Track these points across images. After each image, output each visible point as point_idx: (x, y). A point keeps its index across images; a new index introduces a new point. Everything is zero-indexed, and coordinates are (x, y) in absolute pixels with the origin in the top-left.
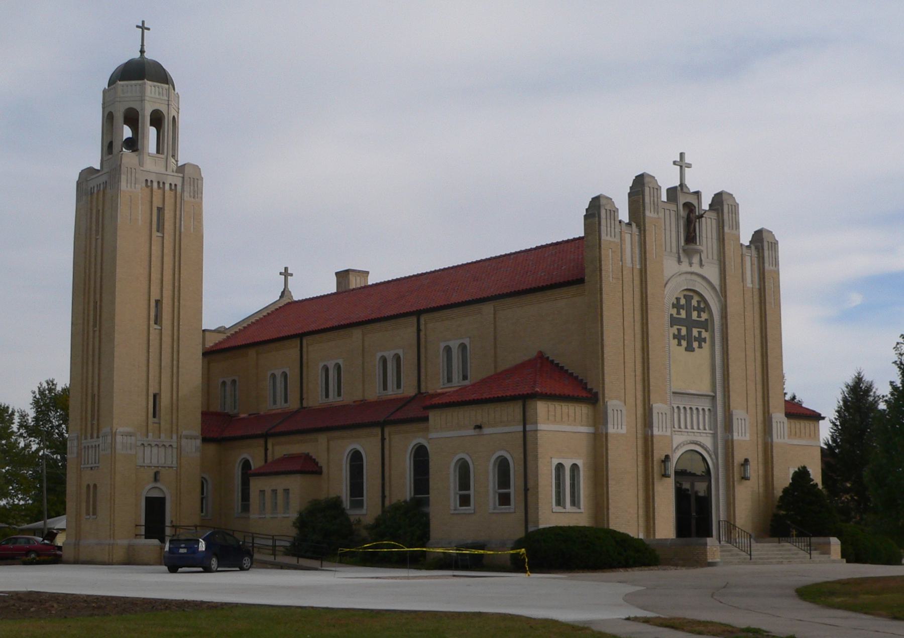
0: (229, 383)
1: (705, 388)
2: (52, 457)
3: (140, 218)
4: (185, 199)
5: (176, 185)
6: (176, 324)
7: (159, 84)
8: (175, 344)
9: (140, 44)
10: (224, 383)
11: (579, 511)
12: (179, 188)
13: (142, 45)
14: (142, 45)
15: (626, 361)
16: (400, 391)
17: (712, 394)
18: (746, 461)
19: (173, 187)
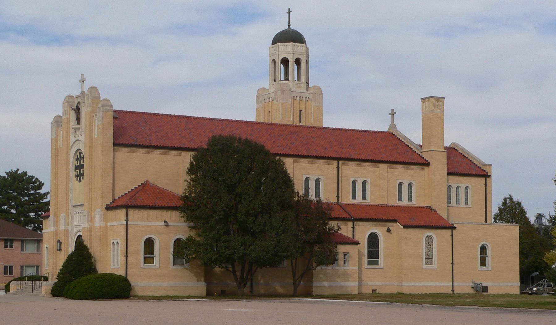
0: (115, 243)
2: (259, 279)
10: (113, 243)
13: (289, 22)
14: (289, 22)
15: (16, 285)
16: (427, 234)
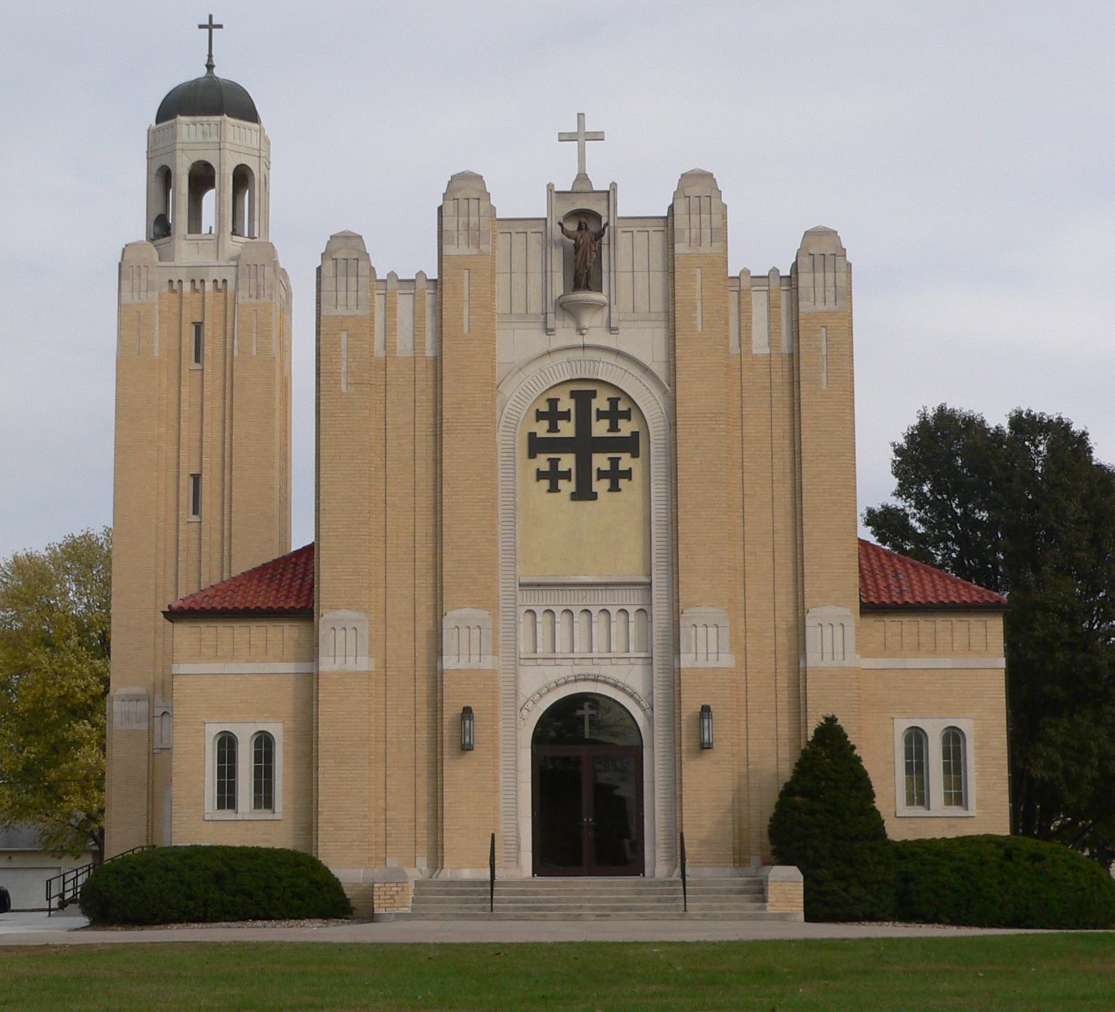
1: (630, 568)
3: (157, 345)
4: (240, 300)
5: (225, 281)
6: (226, 512)
7: (204, 118)
8: (226, 543)
9: (207, 53)
11: (271, 817)
12: (231, 285)
13: (210, 56)
14: (210, 56)
17: (645, 579)
18: (706, 710)
19: (220, 285)
